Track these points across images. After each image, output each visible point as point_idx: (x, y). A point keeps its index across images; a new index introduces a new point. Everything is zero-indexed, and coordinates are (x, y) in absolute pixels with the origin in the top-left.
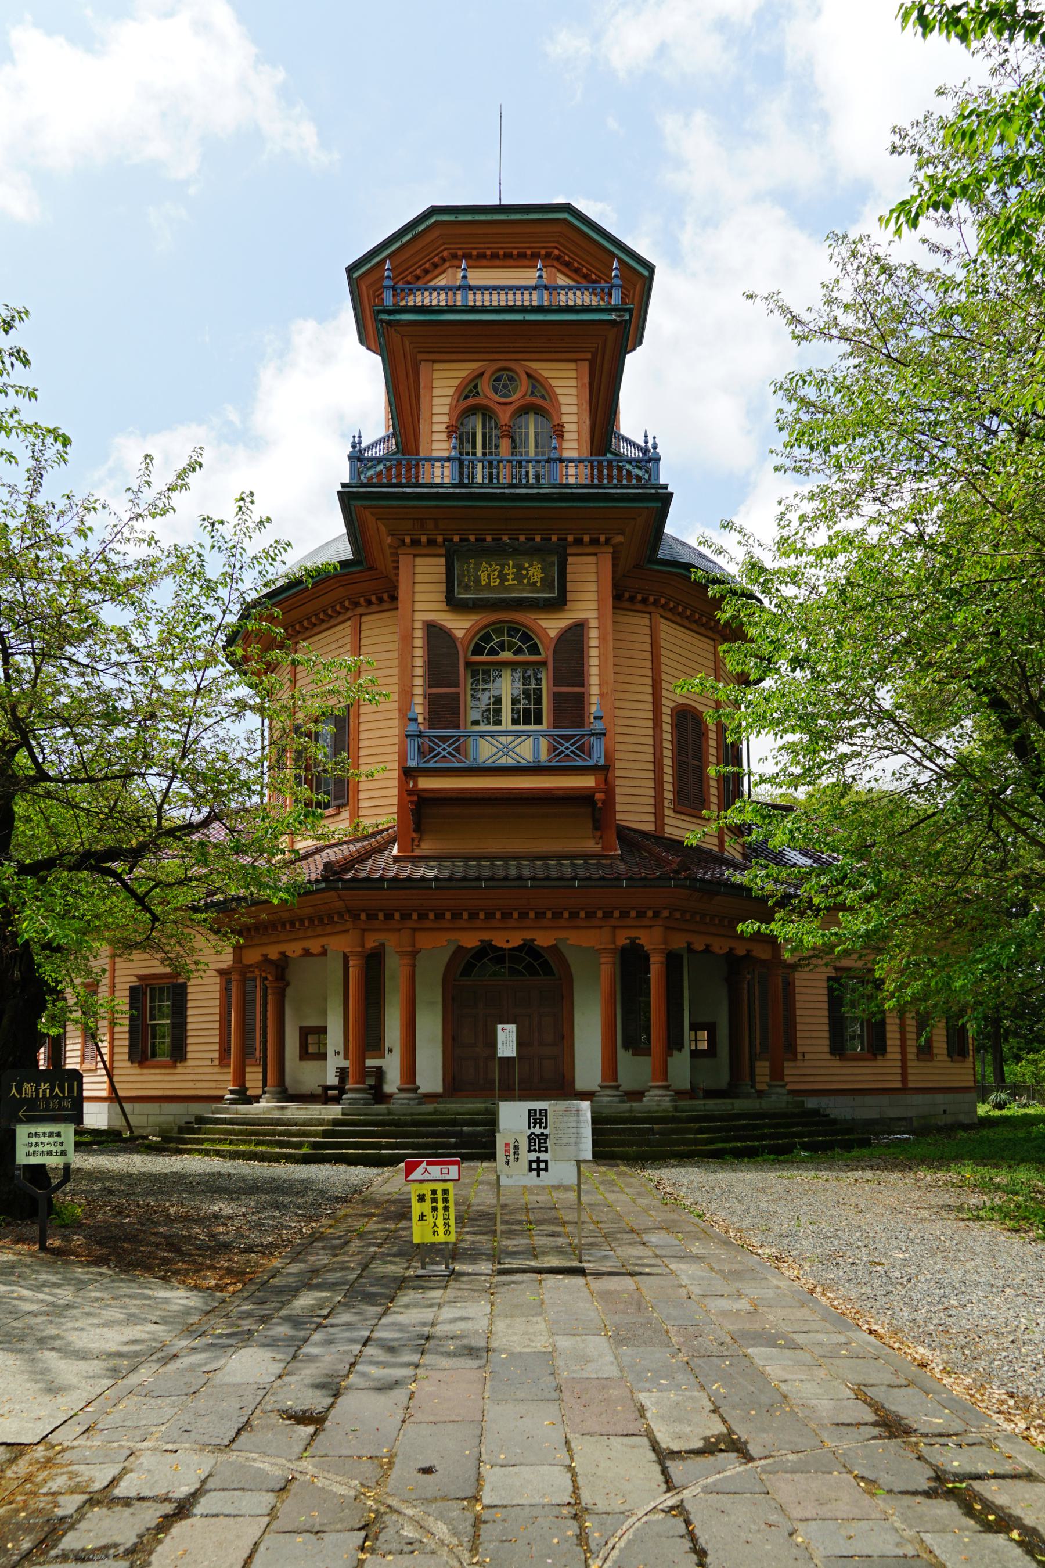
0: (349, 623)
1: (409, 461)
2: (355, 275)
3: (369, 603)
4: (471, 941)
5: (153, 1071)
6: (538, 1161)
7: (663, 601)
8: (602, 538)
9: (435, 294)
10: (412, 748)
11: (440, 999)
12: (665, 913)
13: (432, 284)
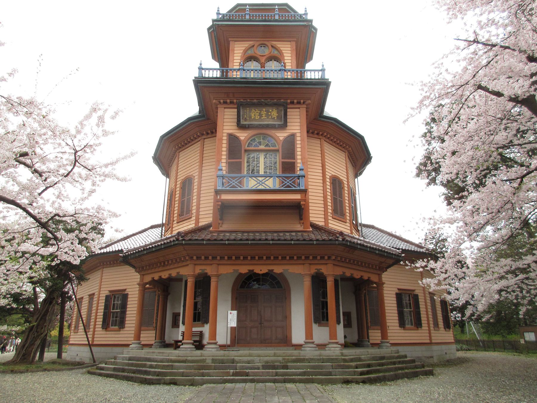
0: (199, 142)
3: (208, 134)
4: (244, 270)
5: (110, 333)
7: (325, 134)
8: (302, 101)
10: (220, 181)
11: (230, 299)
12: (333, 258)
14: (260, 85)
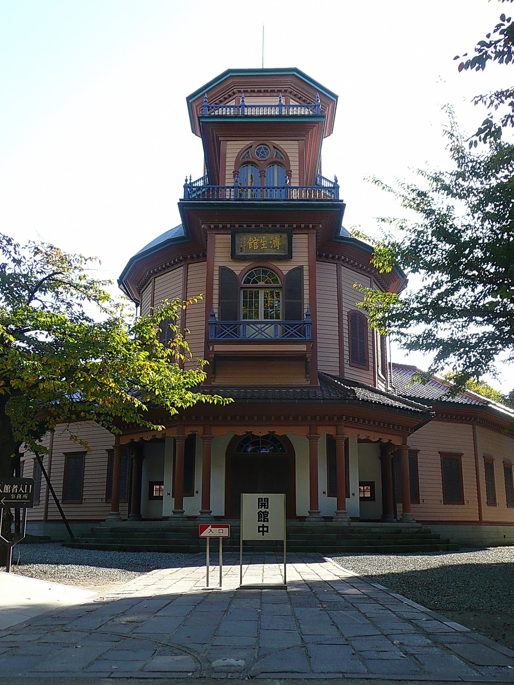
1: (213, 188)
2: (190, 101)
4: (241, 431)
6: (263, 527)
7: (343, 258)
9: (228, 110)
13: (228, 104)
14: (258, 128)
